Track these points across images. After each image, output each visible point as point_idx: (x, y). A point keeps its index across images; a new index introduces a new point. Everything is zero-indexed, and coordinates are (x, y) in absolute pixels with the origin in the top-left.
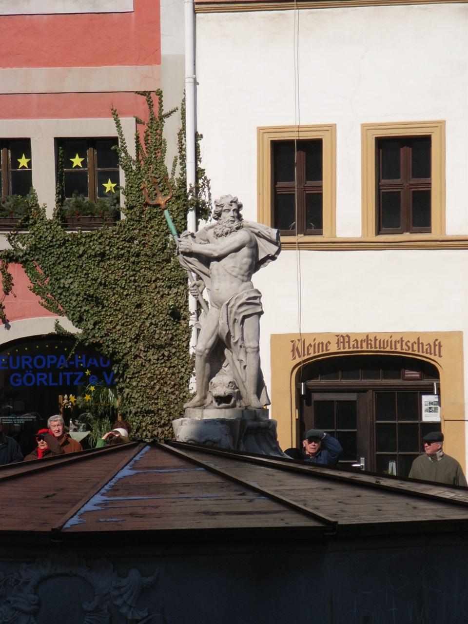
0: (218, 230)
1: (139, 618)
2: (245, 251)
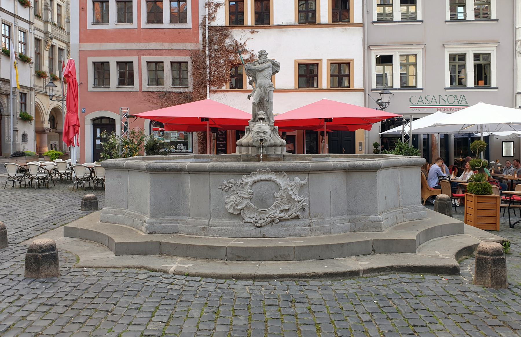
1: (300, 200)
2: (37, 295)
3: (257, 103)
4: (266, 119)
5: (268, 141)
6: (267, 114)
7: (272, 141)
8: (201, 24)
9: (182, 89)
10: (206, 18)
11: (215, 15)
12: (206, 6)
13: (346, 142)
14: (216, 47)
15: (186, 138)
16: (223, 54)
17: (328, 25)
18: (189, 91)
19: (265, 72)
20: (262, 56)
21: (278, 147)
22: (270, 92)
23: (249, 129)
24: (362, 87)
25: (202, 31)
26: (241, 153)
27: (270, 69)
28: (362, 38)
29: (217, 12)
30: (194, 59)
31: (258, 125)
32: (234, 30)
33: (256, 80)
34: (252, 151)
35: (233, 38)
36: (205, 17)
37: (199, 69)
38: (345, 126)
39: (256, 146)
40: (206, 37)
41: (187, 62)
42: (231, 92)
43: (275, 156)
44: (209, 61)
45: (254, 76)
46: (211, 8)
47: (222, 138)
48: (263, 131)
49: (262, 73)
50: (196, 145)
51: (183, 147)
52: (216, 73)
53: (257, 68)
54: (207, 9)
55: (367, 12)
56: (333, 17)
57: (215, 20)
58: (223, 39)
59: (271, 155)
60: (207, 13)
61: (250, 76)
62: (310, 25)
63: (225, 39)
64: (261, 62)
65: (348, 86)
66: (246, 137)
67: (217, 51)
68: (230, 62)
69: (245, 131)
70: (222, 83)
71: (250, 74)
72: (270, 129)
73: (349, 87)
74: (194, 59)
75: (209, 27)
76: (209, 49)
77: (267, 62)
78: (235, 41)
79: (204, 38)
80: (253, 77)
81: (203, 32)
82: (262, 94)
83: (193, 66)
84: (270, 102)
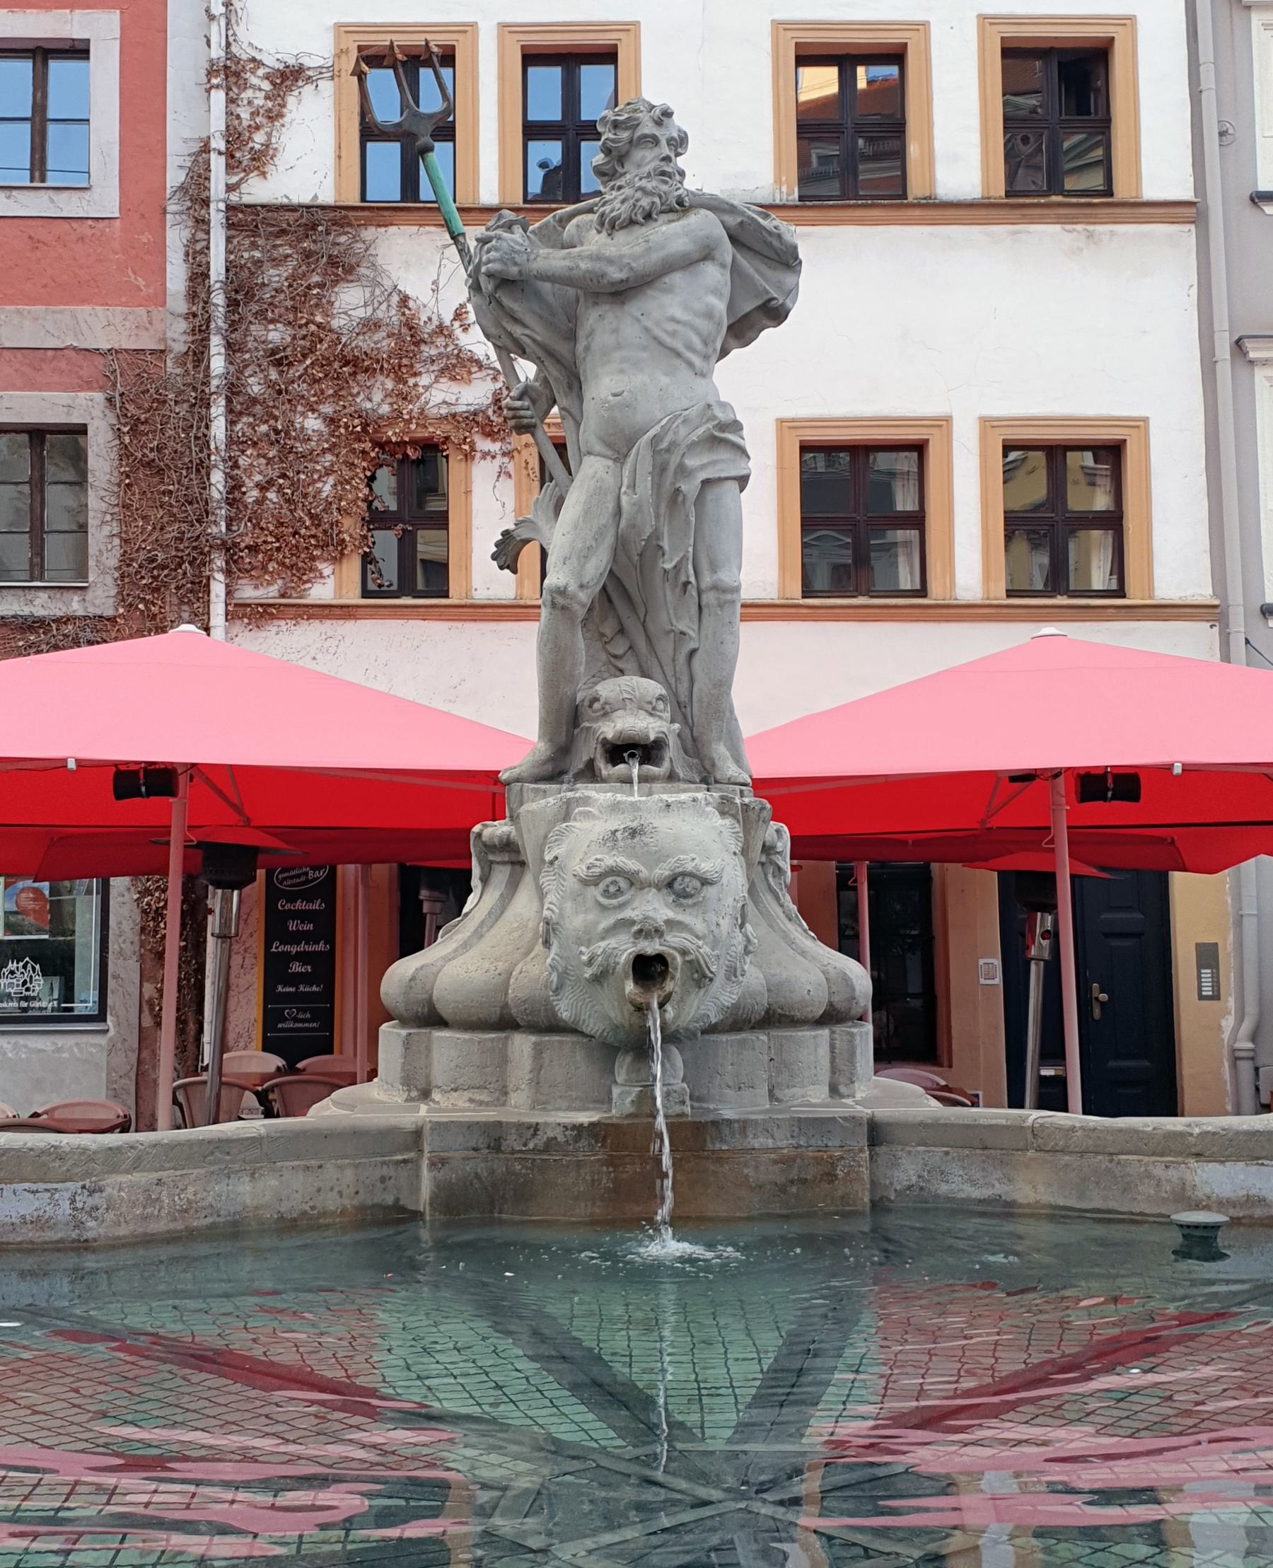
0: (617, 204)
3: (584, 597)
4: (672, 752)
5: (719, 980)
6: (681, 709)
7: (754, 977)
8: (182, 188)
9: (43, 596)
10: (213, 156)
11: (269, 135)
12: (215, 81)
13: (1115, 943)
14: (277, 335)
15: (60, 917)
16: (318, 381)
17: (983, 212)
18: (92, 611)
19: (666, 299)
20: (638, 154)
21: (806, 1034)
22: (711, 495)
23: (508, 847)
24: (1202, 592)
25: (186, 234)
26: (425, 1094)
27: (714, 275)
28: (1194, 290)
29: (286, 120)
30: (131, 408)
31: (615, 807)
32: (392, 229)
33: (575, 382)
34: (536, 1083)
35: (387, 284)
36: (206, 148)
37: (160, 472)
38: (1161, 840)
39: (593, 1025)
40: (213, 273)
41: (82, 430)
42: (371, 617)
43: (783, 1141)
44: (231, 423)
45: (562, 348)
46: (249, 94)
47: (303, 916)
48: (663, 871)
49: (634, 307)
50: (125, 968)
51: (39, 984)
52: (272, 495)
53: (584, 265)
54: (219, 97)
55: (1222, 134)
56: (1010, 154)
57: (268, 168)
58: (321, 286)
59: (744, 1125)
60: (218, 122)
61: (523, 353)
62: (872, 206)
63: (336, 282)
64: (623, 210)
65: (1114, 586)
66: (478, 934)
67: (278, 358)
68: (365, 426)
69: (469, 872)
70: (313, 559)
71: (518, 331)
72: (735, 846)
73: (1120, 593)
74: (131, 408)
75: (231, 208)
76: (232, 348)
77: (681, 207)
78: (395, 299)
79: (199, 276)
80: (551, 354)
81: (192, 240)
82: (638, 506)
83: (125, 453)
84: (715, 587)
